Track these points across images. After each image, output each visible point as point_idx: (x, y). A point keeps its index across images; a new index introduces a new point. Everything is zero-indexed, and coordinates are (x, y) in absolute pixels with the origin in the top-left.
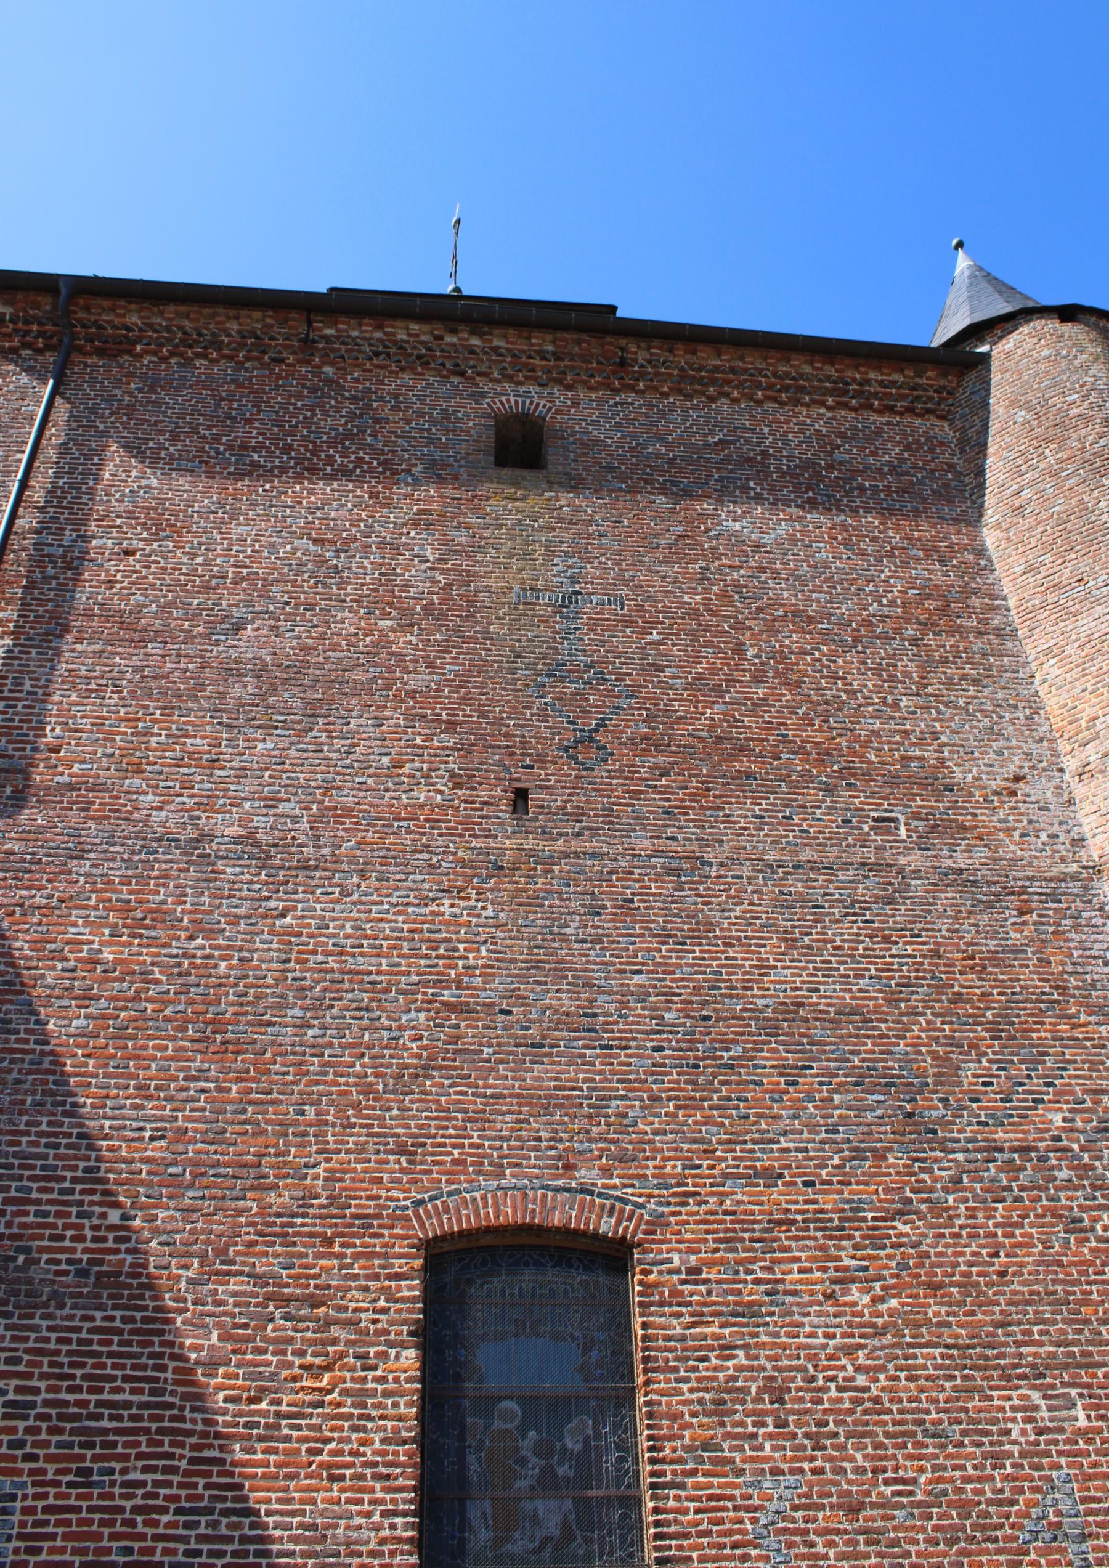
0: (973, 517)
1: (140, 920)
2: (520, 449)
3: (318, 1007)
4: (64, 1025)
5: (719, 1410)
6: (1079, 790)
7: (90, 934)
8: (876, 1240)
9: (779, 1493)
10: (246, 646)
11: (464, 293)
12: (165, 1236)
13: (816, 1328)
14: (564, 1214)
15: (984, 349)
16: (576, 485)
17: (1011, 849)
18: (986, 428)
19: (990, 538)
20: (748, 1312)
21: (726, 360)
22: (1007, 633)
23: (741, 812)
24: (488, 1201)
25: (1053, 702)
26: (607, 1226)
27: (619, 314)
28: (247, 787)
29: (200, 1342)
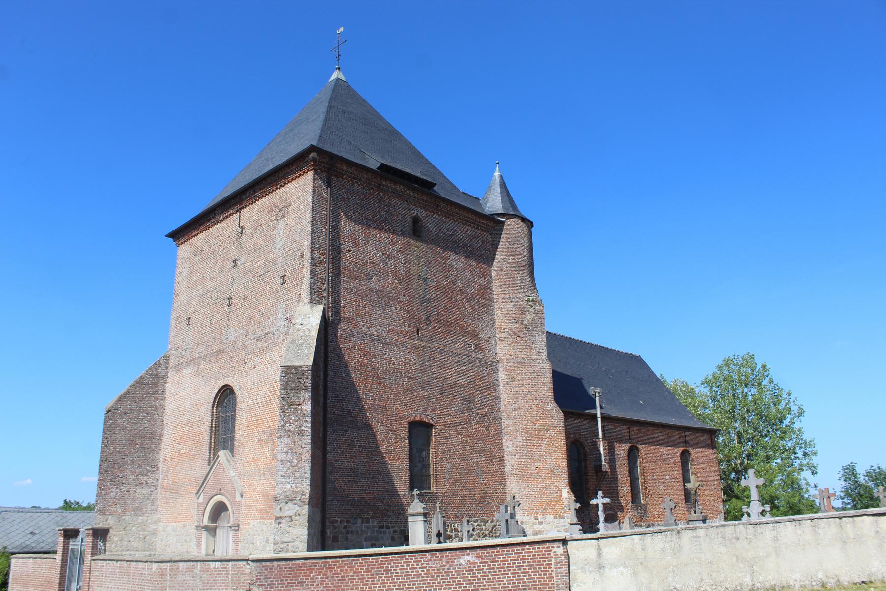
0: (491, 265)
1: (365, 354)
2: (416, 230)
3: (392, 376)
4: (355, 375)
5: (443, 453)
6: (498, 343)
7: (356, 354)
8: (463, 428)
9: (449, 466)
10: (372, 284)
11: (307, 359)
12: (373, 418)
13: (455, 442)
14: (426, 419)
15: (706, 390)
16: (426, 242)
17: (487, 354)
18: (498, 243)
19: (548, 366)
20: (447, 438)
21: (457, 210)
22: (492, 301)
23: (451, 339)
24: (416, 417)
25: (498, 321)
26: (431, 422)
27: (435, 188)
28: (376, 323)
29: (380, 437)
